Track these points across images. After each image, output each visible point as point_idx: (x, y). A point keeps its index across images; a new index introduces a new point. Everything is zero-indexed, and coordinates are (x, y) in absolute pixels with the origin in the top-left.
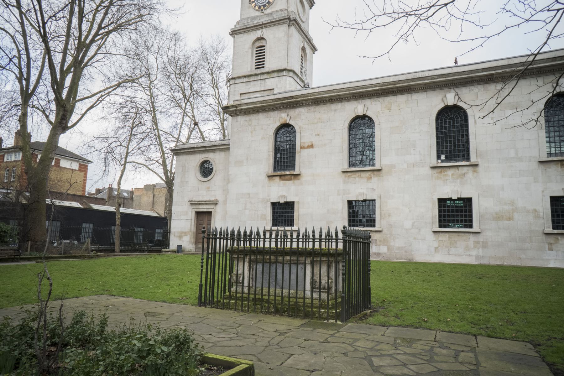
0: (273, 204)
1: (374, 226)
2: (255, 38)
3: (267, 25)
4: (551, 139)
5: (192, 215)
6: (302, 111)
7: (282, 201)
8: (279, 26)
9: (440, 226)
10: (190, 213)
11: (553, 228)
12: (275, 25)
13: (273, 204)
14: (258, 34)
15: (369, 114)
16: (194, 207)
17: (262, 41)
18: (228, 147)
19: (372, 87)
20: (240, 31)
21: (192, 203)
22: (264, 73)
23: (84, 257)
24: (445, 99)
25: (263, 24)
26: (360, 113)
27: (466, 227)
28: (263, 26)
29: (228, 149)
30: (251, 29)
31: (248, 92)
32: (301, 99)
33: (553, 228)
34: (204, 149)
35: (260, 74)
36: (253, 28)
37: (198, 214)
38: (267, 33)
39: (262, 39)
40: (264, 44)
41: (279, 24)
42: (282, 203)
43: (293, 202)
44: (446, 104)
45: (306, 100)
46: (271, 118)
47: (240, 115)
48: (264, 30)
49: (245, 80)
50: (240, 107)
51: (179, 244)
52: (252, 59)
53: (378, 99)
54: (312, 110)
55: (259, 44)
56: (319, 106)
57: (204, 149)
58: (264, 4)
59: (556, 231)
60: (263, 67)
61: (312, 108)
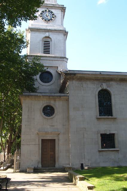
0: (102, 135)
1: (114, 147)
3: (52, 31)
5: (38, 142)
7: (108, 133)
8: (59, 34)
12: (57, 32)
13: (102, 135)
14: (47, 34)
17: (48, 39)
20: (34, 30)
23: (62, 177)
24: (102, 86)
25: (50, 30)
28: (50, 31)
32: (115, 77)
36: (43, 30)
38: (52, 36)
39: (48, 37)
40: (50, 41)
41: (60, 32)
42: (108, 134)
43: (55, 139)
44: (103, 88)
46: (95, 85)
48: (50, 33)
51: (82, 163)
52: (42, 48)
60: (49, 53)
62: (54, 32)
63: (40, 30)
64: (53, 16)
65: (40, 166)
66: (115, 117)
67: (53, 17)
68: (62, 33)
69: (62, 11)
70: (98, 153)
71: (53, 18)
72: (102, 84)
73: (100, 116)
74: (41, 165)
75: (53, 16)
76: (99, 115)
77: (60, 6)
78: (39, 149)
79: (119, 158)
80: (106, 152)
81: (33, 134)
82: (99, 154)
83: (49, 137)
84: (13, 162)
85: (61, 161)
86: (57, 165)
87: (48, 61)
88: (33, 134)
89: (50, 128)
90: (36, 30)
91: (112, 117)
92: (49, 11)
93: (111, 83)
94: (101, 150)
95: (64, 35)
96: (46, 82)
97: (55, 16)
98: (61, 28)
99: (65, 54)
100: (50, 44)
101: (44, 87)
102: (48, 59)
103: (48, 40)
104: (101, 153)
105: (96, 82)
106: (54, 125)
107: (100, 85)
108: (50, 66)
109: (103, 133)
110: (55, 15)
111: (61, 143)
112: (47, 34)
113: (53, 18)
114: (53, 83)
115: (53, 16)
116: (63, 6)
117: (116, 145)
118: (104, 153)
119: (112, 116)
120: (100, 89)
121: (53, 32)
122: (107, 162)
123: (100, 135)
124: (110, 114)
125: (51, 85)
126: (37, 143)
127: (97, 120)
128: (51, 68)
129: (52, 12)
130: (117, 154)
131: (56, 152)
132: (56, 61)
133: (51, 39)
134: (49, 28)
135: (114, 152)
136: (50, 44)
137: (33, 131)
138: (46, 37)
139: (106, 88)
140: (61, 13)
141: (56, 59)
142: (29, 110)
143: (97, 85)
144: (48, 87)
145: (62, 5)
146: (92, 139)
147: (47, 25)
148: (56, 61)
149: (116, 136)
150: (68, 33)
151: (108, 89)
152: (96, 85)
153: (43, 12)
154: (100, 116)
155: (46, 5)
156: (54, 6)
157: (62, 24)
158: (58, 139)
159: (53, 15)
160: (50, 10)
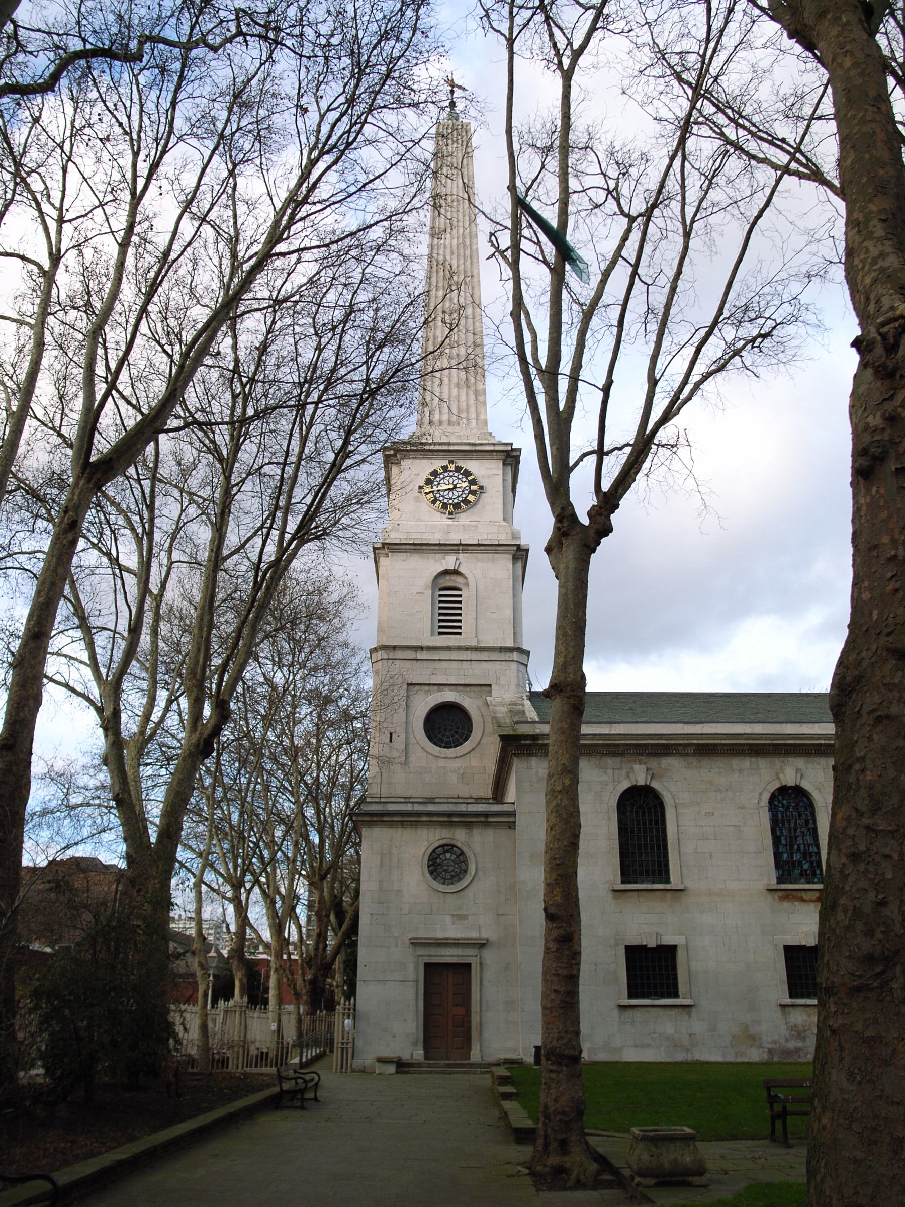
1: (676, 995)
2: (441, 569)
3: (470, 548)
4: (449, 728)
5: (414, 972)
6: (671, 763)
7: (652, 944)
9: (631, 996)
10: (411, 967)
11: (791, 997)
12: (482, 551)
14: (449, 562)
15: (806, 785)
16: (421, 951)
17: (454, 577)
18: (512, 819)
19: (812, 739)
21: (416, 944)
22: (459, 648)
25: (460, 544)
26: (791, 783)
27: (669, 996)
28: (461, 548)
29: (512, 826)
30: (432, 547)
31: (428, 682)
33: (791, 997)
34: (446, 819)
35: (449, 648)
36: (436, 548)
37: (431, 968)
38: (468, 565)
40: (460, 586)
41: (496, 552)
45: (685, 746)
46: (608, 771)
47: (536, 756)
49: (410, 654)
50: (543, 739)
53: (817, 760)
54: (694, 764)
55: (449, 581)
56: (706, 759)
57: (446, 819)
58: (456, 501)
59: (634, 1002)
60: (460, 633)
61: (694, 761)
62: (477, 551)
63: (424, 547)
64: (474, 488)
65: (419, 1054)
66: (681, 887)
67: (473, 493)
68: (506, 552)
69: (504, 464)
70: (616, 1013)
71: (471, 498)
72: (632, 768)
73: (623, 882)
74: (422, 1052)
75: (477, 489)
76: (619, 878)
77: (497, 448)
78: (417, 994)
79: (690, 1035)
80: (645, 1009)
81: (397, 947)
82: (620, 1017)
83: (449, 955)
84: (878, 717)
85: (823, 978)
86: (475, 1056)
87: (454, 665)
88: (397, 947)
89: (453, 924)
90: (408, 547)
91: (668, 887)
92: (458, 469)
93: (666, 762)
94: (627, 1002)
95: (515, 559)
96: (448, 746)
97: (481, 488)
98: (504, 539)
99: (516, 633)
100: (460, 596)
101: (442, 763)
102: (455, 655)
103: (455, 582)
104: (629, 1013)
105: (610, 761)
106: (467, 916)
107: (624, 772)
108: (463, 683)
109: (636, 943)
110: (482, 482)
111: (488, 975)
112: (449, 562)
113: (471, 498)
114: (473, 749)
115: (474, 488)
116: (509, 448)
117: (682, 988)
118: (638, 1014)
119: (668, 881)
120: (625, 785)
121: (472, 551)
122: (649, 1045)
123: (622, 951)
124: (660, 874)
125: (469, 752)
126: (411, 976)
127: (615, 898)
128: (468, 689)
129: (467, 473)
130: (687, 1017)
131: (475, 1008)
132: (484, 664)
133: (466, 578)
134: (454, 538)
135: (673, 1012)
136: (460, 596)
137: (396, 935)
138: (446, 572)
139: (648, 783)
140: (501, 472)
141: (485, 656)
142: (381, 865)
143: (617, 772)
144: (457, 764)
145: (506, 444)
146: (596, 964)
147: (448, 525)
148: (485, 665)
149: (681, 956)
150: (527, 551)
151: (655, 785)
152: (610, 772)
153: (435, 473)
154: (623, 882)
155: (445, 448)
156: (473, 448)
157: (507, 517)
158: (481, 964)
159: (473, 482)
160: (460, 463)
